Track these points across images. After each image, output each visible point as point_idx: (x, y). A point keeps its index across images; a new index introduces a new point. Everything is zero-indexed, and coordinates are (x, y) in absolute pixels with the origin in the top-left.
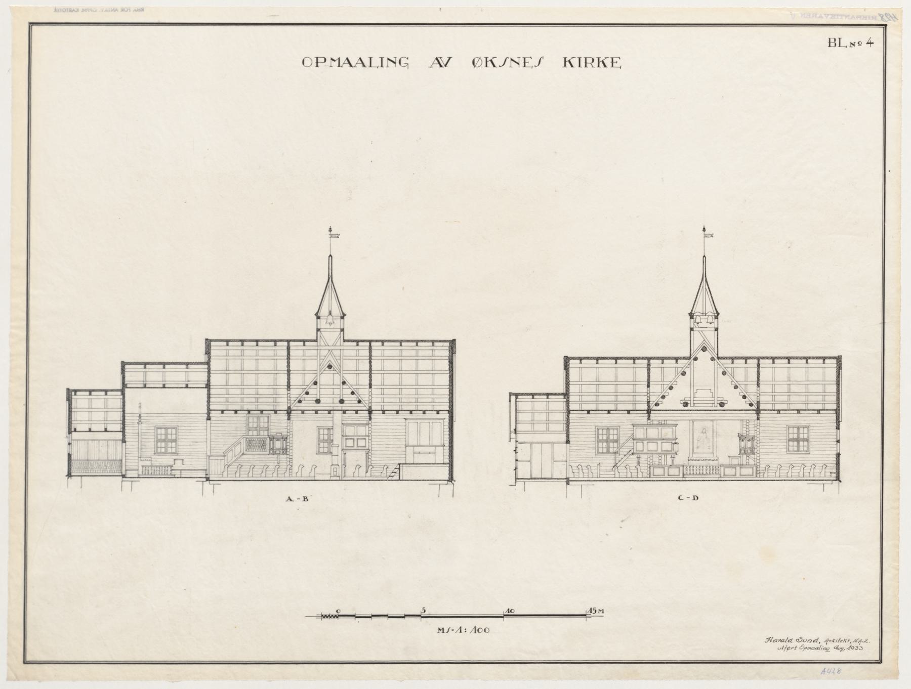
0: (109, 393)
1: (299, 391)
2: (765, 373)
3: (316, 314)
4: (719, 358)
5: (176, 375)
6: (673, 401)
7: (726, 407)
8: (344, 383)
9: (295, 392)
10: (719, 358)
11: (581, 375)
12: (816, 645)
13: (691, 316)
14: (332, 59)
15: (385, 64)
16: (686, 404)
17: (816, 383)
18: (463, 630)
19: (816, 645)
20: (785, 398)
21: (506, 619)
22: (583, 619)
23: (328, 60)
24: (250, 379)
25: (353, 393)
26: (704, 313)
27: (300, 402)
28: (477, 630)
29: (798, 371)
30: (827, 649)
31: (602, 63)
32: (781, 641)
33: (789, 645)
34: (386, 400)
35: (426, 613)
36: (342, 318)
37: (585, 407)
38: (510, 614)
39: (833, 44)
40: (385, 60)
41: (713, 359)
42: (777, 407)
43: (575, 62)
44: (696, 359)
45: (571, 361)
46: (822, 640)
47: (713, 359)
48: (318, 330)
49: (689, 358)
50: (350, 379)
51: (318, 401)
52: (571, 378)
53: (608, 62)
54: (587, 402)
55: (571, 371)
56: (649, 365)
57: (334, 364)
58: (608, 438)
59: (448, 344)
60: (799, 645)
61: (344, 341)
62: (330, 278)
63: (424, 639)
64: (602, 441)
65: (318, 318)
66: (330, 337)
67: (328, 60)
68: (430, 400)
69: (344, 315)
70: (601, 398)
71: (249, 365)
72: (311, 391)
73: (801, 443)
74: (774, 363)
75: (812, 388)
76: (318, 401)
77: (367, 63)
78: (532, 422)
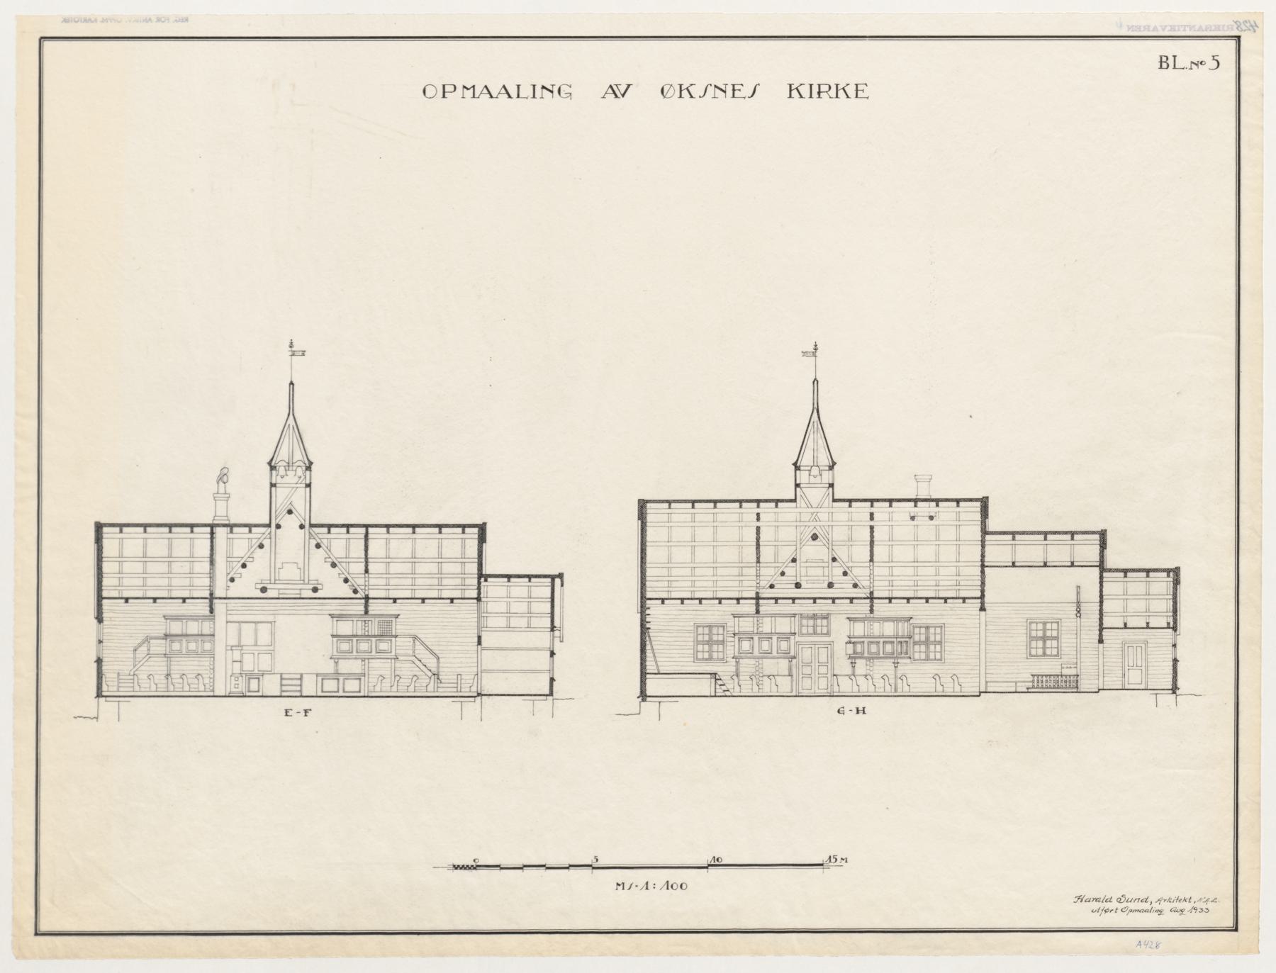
0: (1129, 574)
1: (771, 571)
2: (376, 548)
3: (270, 463)
4: (312, 526)
5: (1059, 551)
6: (246, 585)
7: (270, 594)
8: (834, 560)
9: (768, 573)
10: (312, 526)
11: (464, 547)
12: (1146, 906)
13: (797, 467)
14: (543, 87)
15: (538, 93)
16: (264, 590)
17: (451, 560)
18: (650, 886)
19: (1146, 906)
20: (140, 582)
21: (712, 870)
22: (818, 870)
23: (459, 88)
24: (704, 555)
25: (845, 574)
26: (291, 463)
27: (772, 586)
28: (669, 886)
29: (427, 543)
30: (1160, 912)
31: (684, 90)
32: (1097, 900)
33: (1107, 905)
34: (719, 584)
35: (600, 863)
36: (831, 468)
37: (446, 594)
38: (716, 864)
39: (1164, 65)
40: (538, 89)
41: (302, 527)
42: (394, 594)
43: (805, 90)
44: (278, 526)
45: (105, 530)
46: (1153, 898)
47: (302, 527)
48: (797, 485)
49: (269, 526)
50: (842, 553)
51: (798, 586)
52: (105, 553)
53: (851, 90)
54: (397, 587)
55: (105, 542)
56: (212, 533)
57: (818, 531)
58: (927, 638)
59: (978, 504)
60: (1121, 906)
61: (834, 500)
62: (291, 411)
63: (593, 899)
64: (1037, 639)
65: (273, 468)
66: (816, 495)
67: (459, 88)
68: (711, 584)
69: (834, 463)
70: (419, 582)
71: (705, 534)
72: (788, 571)
73: (1049, 643)
74: (121, 531)
75: (448, 568)
76: (798, 586)
77: (513, 93)
78: (509, 614)
